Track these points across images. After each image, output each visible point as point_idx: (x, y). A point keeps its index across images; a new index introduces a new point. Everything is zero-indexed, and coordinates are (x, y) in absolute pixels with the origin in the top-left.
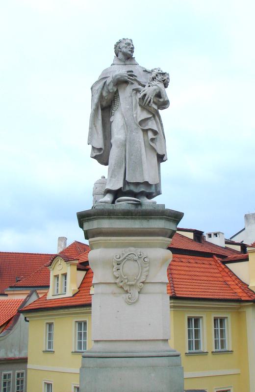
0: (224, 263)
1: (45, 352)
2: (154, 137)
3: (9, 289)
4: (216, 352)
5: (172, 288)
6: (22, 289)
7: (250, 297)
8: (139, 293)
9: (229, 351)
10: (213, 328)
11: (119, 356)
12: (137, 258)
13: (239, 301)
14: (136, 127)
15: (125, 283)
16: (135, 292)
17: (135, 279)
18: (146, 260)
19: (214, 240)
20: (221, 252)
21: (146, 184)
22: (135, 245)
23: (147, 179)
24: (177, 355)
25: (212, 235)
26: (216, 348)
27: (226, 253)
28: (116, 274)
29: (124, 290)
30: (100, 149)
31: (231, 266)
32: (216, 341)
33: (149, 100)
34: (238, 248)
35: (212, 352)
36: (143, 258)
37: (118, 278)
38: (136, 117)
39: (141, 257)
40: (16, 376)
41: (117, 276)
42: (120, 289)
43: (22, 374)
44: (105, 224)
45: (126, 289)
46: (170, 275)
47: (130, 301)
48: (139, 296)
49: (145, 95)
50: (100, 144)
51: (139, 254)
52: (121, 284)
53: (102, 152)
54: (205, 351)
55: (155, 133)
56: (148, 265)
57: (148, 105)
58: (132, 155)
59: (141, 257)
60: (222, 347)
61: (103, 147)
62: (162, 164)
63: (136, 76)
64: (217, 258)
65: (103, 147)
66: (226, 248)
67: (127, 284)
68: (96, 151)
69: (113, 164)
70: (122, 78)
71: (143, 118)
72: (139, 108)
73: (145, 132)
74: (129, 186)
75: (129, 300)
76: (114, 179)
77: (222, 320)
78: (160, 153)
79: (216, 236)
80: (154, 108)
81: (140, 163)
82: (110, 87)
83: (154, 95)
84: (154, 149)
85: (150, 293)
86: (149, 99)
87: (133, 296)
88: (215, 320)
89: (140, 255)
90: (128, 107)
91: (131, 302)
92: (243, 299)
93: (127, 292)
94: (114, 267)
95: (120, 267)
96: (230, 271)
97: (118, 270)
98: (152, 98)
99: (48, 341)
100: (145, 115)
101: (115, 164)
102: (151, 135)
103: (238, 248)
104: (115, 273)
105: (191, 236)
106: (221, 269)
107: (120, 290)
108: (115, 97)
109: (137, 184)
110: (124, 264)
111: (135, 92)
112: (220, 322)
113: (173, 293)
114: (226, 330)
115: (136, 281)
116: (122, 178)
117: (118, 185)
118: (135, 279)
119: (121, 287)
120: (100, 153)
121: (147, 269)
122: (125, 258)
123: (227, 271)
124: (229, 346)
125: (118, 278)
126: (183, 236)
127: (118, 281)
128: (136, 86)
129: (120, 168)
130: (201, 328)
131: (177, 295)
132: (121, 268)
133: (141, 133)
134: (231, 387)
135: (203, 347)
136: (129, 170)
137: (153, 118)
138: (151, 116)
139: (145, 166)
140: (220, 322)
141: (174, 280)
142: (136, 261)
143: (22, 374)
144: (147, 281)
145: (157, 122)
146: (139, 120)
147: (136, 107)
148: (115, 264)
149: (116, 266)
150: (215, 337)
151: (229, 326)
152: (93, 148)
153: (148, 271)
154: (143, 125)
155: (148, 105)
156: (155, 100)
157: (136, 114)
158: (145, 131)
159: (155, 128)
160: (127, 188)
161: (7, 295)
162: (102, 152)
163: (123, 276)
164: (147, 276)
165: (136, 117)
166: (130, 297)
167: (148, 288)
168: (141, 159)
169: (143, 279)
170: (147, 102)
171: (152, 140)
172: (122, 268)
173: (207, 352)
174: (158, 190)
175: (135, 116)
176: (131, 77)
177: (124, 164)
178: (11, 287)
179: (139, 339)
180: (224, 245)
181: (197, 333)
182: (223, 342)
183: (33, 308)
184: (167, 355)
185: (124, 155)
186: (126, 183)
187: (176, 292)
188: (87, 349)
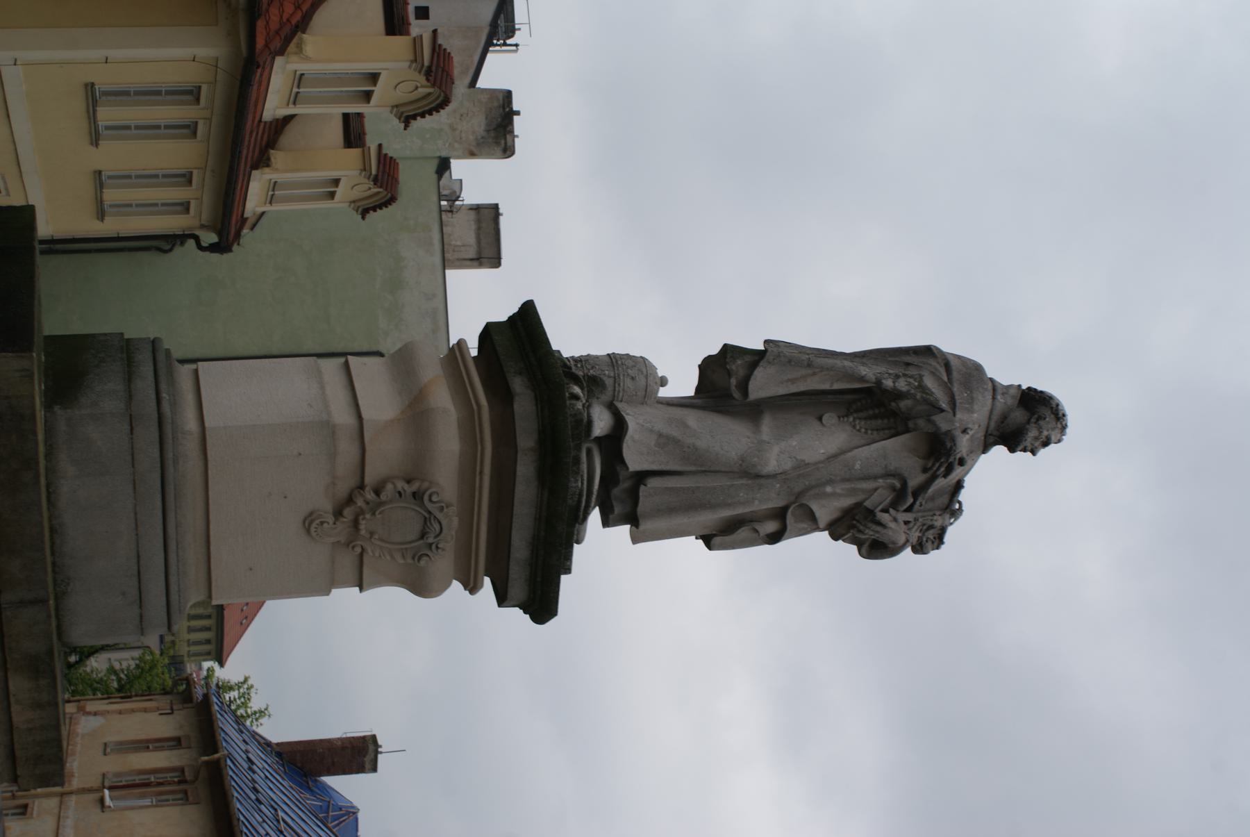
1: (89, 88)
7: (267, 46)
12: (431, 540)
30: (744, 387)
36: (429, 553)
67: (361, 517)
71: (818, 514)
90: (857, 466)
91: (309, 522)
92: (260, 24)
93: (338, 513)
94: (409, 482)
97: (400, 493)
99: (160, 202)
101: (697, 449)
104: (389, 486)
107: (343, 489)
110: (414, 510)
116: (655, 467)
120: (733, 388)
122: (430, 513)
133: (780, 503)
147: (853, 492)
148: (415, 486)
149: (409, 489)
157: (834, 494)
166: (325, 525)
175: (829, 489)
177: (693, 468)
179: (212, 548)
188: (108, 181)
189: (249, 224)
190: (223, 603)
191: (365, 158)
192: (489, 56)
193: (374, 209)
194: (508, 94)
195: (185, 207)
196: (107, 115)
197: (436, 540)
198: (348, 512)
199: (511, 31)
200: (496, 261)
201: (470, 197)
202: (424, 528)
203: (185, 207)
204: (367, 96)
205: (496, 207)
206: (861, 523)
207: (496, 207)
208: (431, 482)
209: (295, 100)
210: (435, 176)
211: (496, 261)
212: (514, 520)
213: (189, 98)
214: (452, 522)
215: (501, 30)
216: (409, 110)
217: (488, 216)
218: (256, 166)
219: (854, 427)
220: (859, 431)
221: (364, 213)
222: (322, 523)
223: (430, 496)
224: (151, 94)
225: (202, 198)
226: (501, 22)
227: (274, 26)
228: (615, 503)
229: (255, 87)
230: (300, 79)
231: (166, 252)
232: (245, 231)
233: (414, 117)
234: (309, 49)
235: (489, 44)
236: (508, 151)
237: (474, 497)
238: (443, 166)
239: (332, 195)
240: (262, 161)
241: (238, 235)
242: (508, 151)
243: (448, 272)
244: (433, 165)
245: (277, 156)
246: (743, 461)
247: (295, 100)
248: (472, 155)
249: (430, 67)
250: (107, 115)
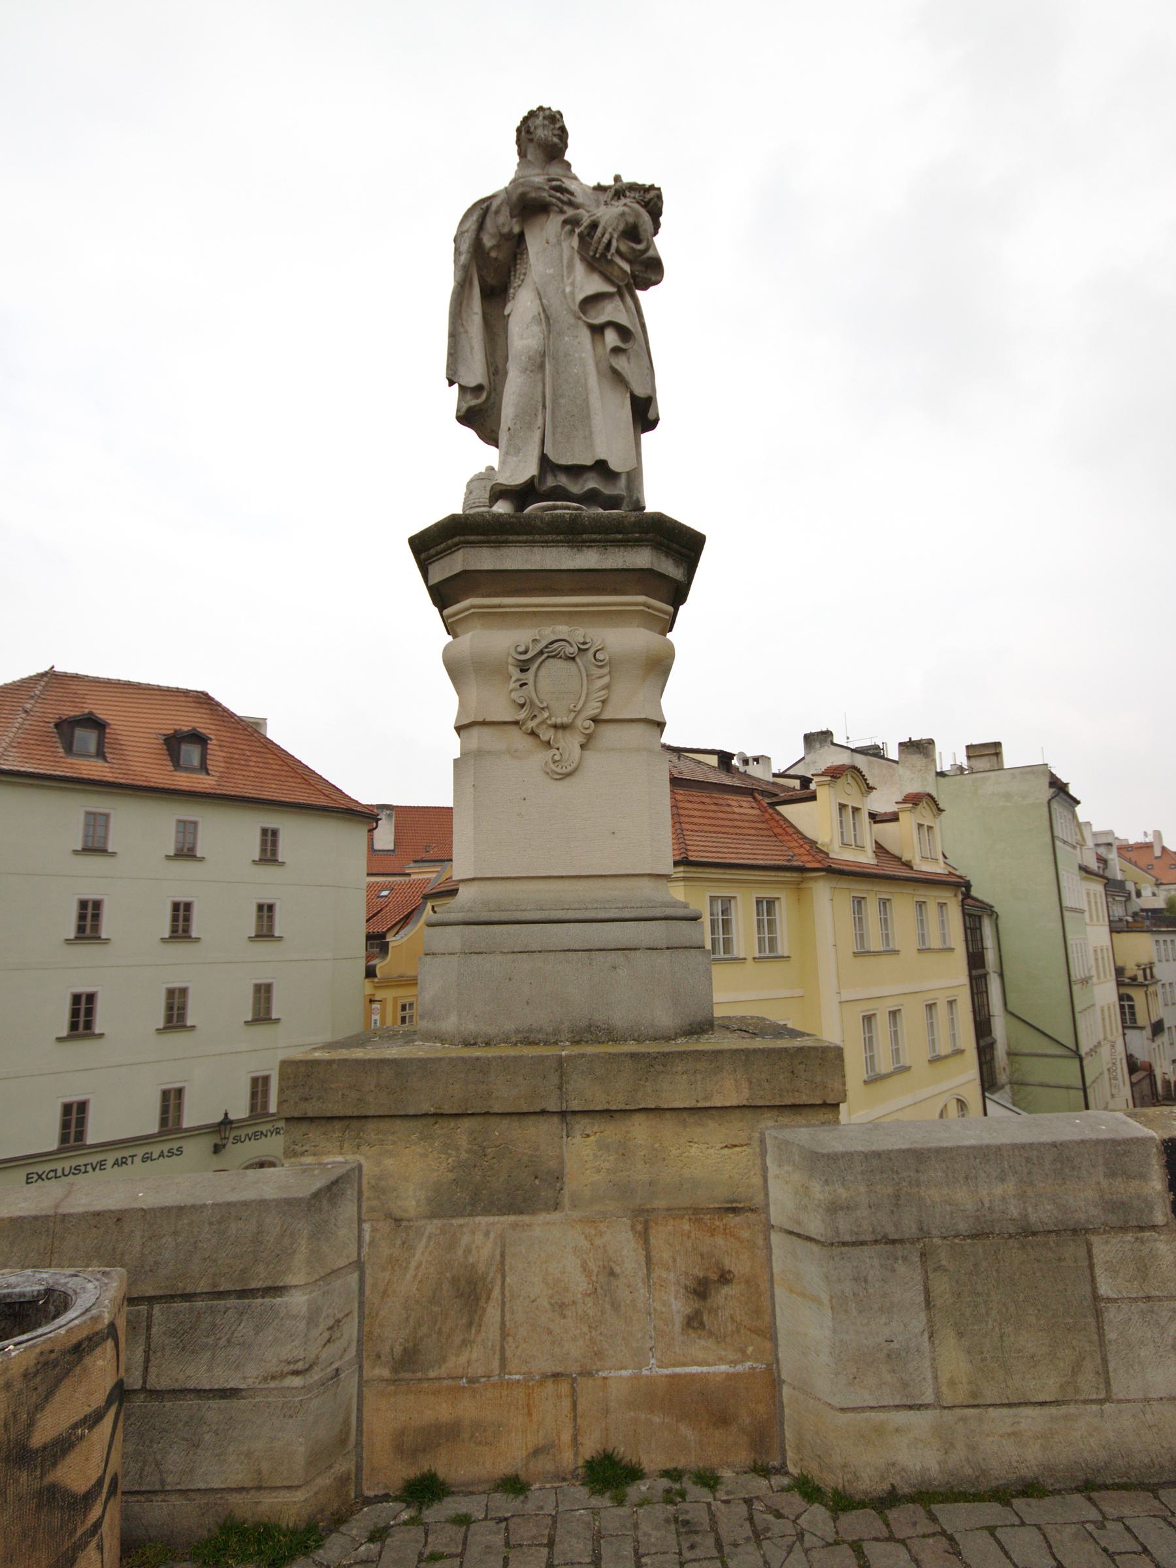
0: (772, 805)
2: (620, 344)
3: (412, 865)
4: (760, 958)
5: (682, 845)
6: (432, 864)
7: (820, 862)
8: (582, 747)
9: (783, 957)
10: (755, 918)
11: (524, 918)
13: (801, 870)
14: (572, 321)
15: (543, 722)
16: (570, 743)
17: (571, 711)
18: (600, 656)
19: (754, 770)
20: (770, 789)
21: (601, 468)
22: (573, 616)
23: (601, 452)
24: (692, 915)
25: (751, 761)
26: (760, 952)
27: (776, 790)
28: (520, 698)
29: (542, 742)
30: (479, 389)
31: (785, 810)
32: (759, 939)
33: (605, 240)
34: (796, 783)
35: (754, 958)
37: (522, 706)
38: (572, 293)
39: (587, 650)
40: (400, 1008)
41: (522, 701)
42: (530, 739)
43: (411, 1005)
44: (485, 559)
45: (544, 738)
46: (678, 825)
47: (559, 770)
48: (581, 758)
49: (594, 226)
50: (475, 374)
51: (40, 1180)
52: (531, 724)
53: (484, 396)
54: (741, 957)
55: (624, 333)
56: (606, 670)
57: (604, 255)
58: (562, 396)
59: (587, 650)
60: (772, 949)
61: (485, 382)
62: (645, 437)
63: (572, 194)
64: (760, 798)
65: (485, 382)
66: (774, 783)
68: (469, 397)
69: (511, 416)
70: (533, 195)
72: (580, 268)
73: (597, 337)
74: (555, 476)
75: (553, 767)
76: (514, 459)
77: (771, 903)
78: (640, 392)
79: (758, 763)
80: (620, 268)
81: (585, 416)
82: (505, 211)
83: (621, 227)
84: (618, 377)
85: (841, 816)
86: (607, 236)
87: (566, 756)
88: (759, 902)
89: (584, 643)
90: (551, 271)
92: (808, 865)
95: (529, 676)
96: (786, 820)
97: (522, 685)
98: (615, 236)
100: (595, 285)
101: (516, 416)
102: (611, 338)
103: (796, 783)
105: (713, 760)
106: (767, 816)
107: (529, 742)
108: (516, 245)
109: (576, 471)
111: (568, 227)
112: (767, 906)
113: (683, 855)
114: (778, 921)
115: (573, 714)
117: (525, 470)
118: (571, 711)
119: (533, 733)
120: (479, 401)
121: (606, 680)
122: (541, 653)
123: (778, 818)
124: (783, 948)
125: (522, 706)
126: (699, 762)
127: (522, 715)
128: (570, 212)
129: (530, 426)
130: (733, 917)
131: (691, 859)
132: (531, 681)
133: (585, 335)
134: (789, 1019)
135: (739, 950)
136: (554, 434)
137: (617, 298)
138: (612, 289)
139: (598, 422)
140: (767, 906)
141: (683, 819)
142: (573, 659)
143: (411, 1005)
144: (605, 716)
145: (627, 310)
146: (580, 296)
147: (571, 267)
149: (515, 673)
150: (759, 933)
151: (784, 912)
152: (462, 388)
153: (607, 687)
154: (592, 313)
155: (604, 255)
156: (623, 248)
157: (573, 284)
158: (597, 330)
159: (623, 320)
160: (550, 482)
161: (409, 875)
162: (484, 396)
163: (537, 701)
164: (603, 702)
165: (572, 293)
166: (557, 758)
167: (609, 734)
168: (588, 403)
169: (593, 709)
170: (601, 247)
171: (616, 350)
172: (535, 681)
173: (745, 959)
174: (635, 498)
175: (568, 290)
176: (558, 195)
178: (415, 861)
180: (771, 779)
181: (771, 923)
182: (772, 941)
183: (445, 889)
184: (662, 915)
185: (540, 394)
186: (544, 460)
187: (690, 853)
189: (954, 871)
190: (454, 863)
191: (903, 810)
192: (890, 757)
193: (937, 805)
194: (901, 744)
195: (942, 906)
196: (875, 943)
197: (575, 645)
198: (546, 734)
199: (876, 747)
200: (997, 745)
201: (963, 760)
202: (561, 658)
203: (942, 906)
204: (856, 810)
205: (967, 747)
206: (597, 249)
207: (967, 747)
208: (509, 654)
209: (861, 848)
210: (947, 778)
211: (997, 745)
212: (548, 568)
213: (863, 903)
214: (549, 632)
215: (876, 751)
216: (864, 788)
217: (973, 751)
218: (911, 868)
219: (519, 286)
220: (522, 281)
221: (940, 810)
222: (555, 762)
223: (521, 653)
224: (859, 921)
225: (932, 897)
226: (871, 752)
227: (810, 858)
228: (586, 488)
229: (865, 870)
230: (845, 844)
231: (997, 916)
232: (957, 873)
233: (867, 784)
234: (827, 840)
235: (883, 757)
236: (931, 742)
237: (534, 612)
238: (942, 774)
239: (930, 828)
240: (908, 865)
241: (960, 877)
242: (931, 742)
243: (1005, 767)
244: (940, 779)
245: (906, 857)
246: (526, 370)
247: (861, 848)
248: (934, 761)
249: (832, 777)
250: (875, 943)
